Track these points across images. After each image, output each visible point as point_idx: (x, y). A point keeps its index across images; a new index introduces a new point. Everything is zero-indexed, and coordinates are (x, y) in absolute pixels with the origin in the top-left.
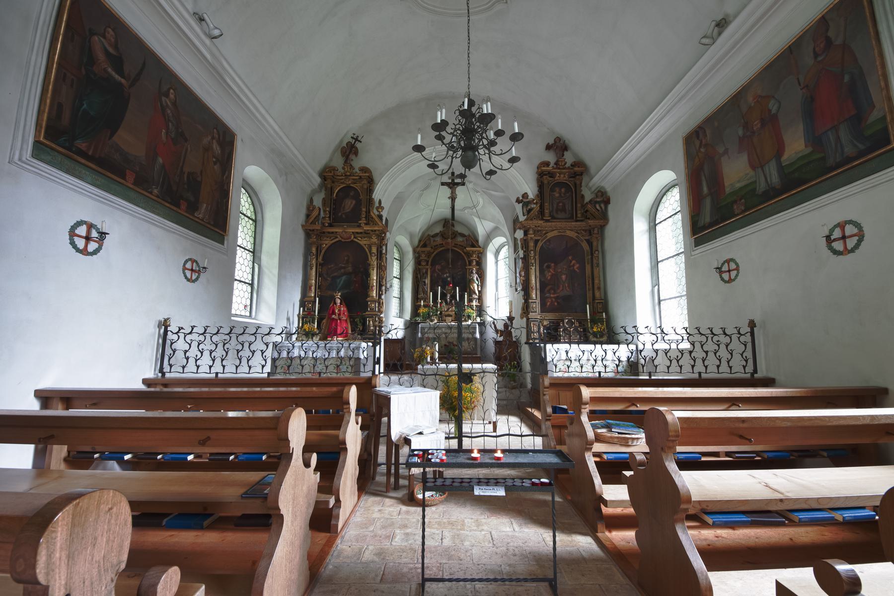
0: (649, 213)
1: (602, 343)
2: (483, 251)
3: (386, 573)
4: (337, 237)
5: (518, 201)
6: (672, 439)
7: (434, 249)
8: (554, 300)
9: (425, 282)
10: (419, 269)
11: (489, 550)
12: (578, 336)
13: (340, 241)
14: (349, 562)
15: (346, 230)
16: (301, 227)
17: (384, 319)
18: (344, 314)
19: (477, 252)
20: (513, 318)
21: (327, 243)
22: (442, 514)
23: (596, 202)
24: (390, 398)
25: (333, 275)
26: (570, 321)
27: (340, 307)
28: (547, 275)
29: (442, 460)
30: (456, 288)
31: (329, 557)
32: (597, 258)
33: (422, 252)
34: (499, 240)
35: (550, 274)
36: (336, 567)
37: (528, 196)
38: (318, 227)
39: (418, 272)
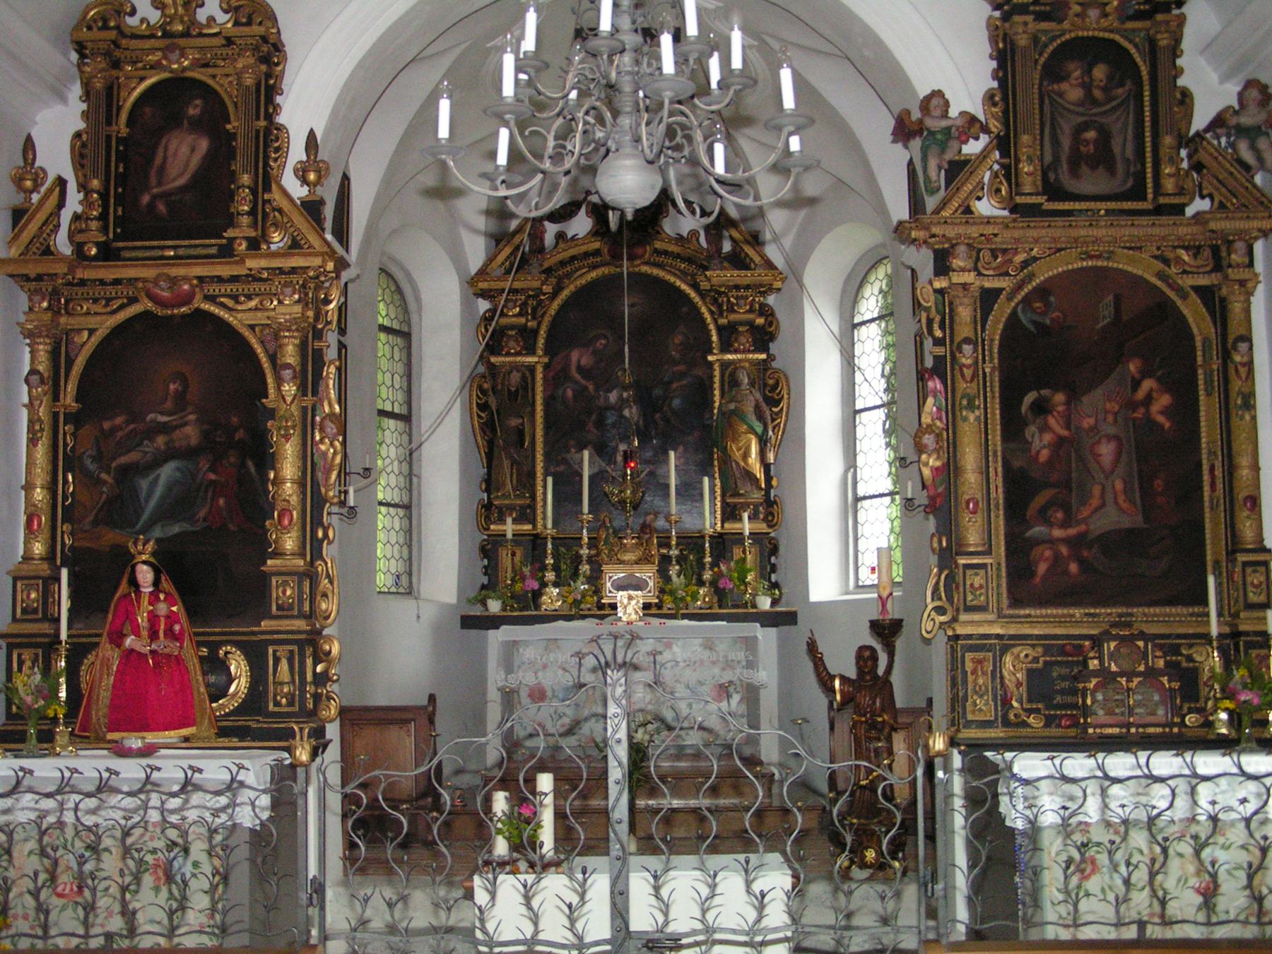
4: (133, 300)
8: (1064, 550)
25: (123, 460)
28: (1036, 444)
35: (1047, 437)
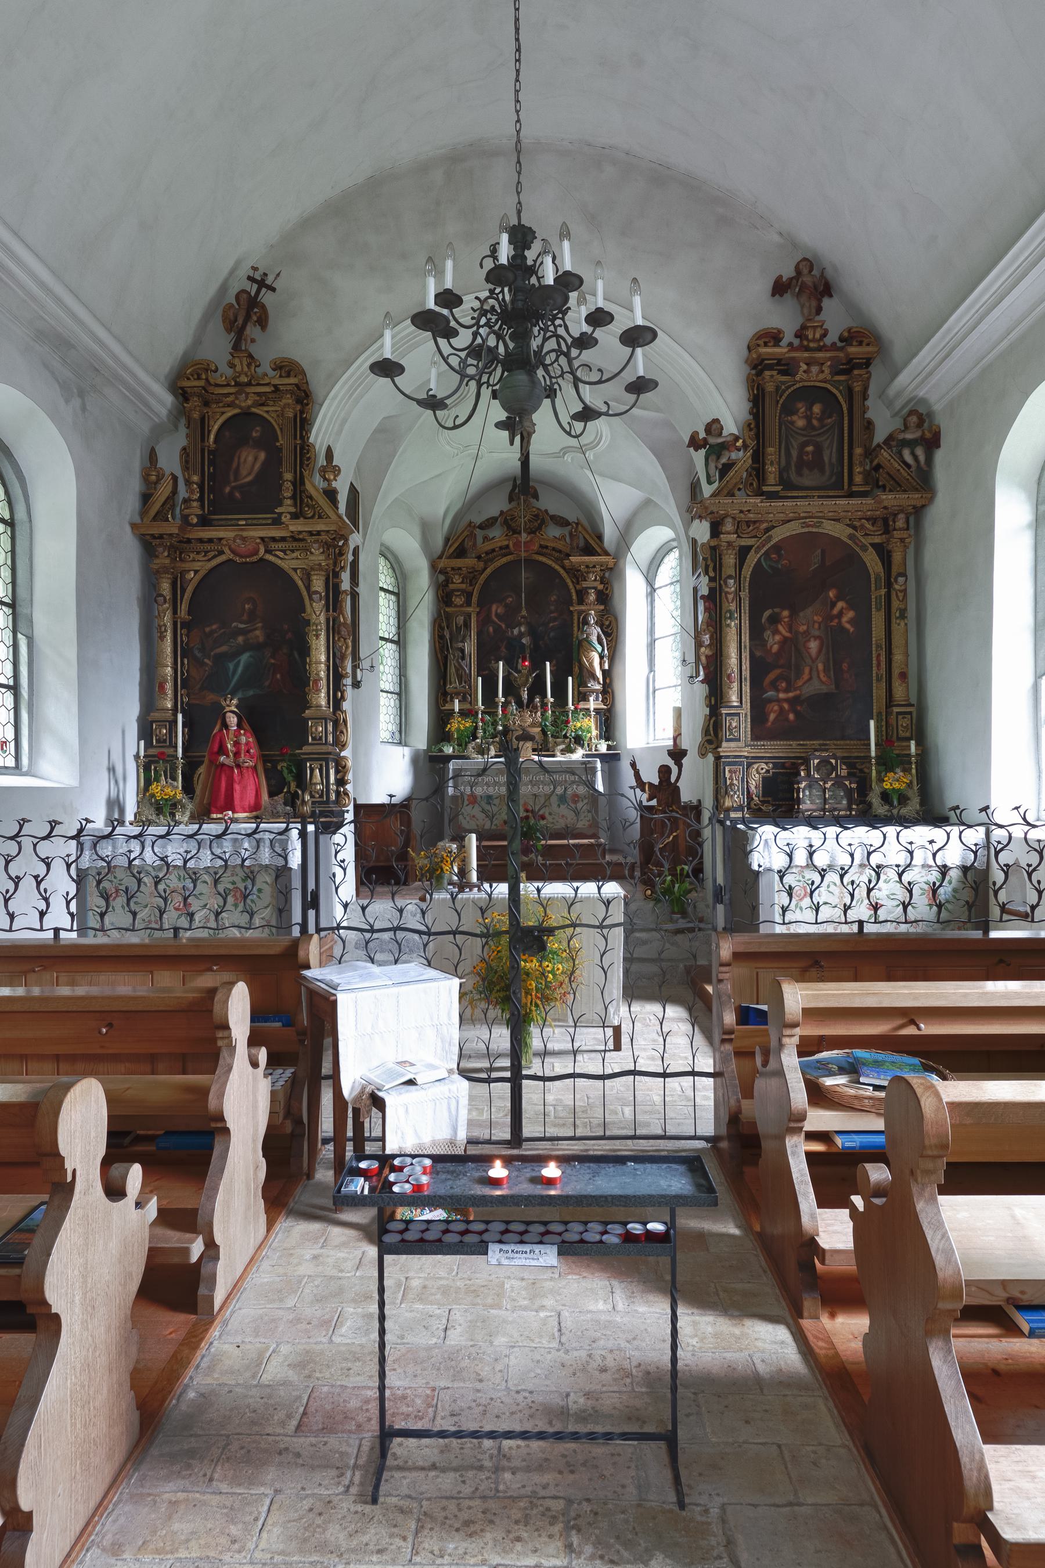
0: (1037, 476)
1: (905, 822)
2: (615, 564)
3: (311, 1409)
4: (222, 553)
5: (695, 443)
6: (930, 1153)
7: (486, 562)
8: (786, 706)
9: (462, 651)
10: (448, 617)
11: (549, 1357)
12: (845, 802)
13: (230, 560)
14: (233, 1382)
15: (245, 534)
16: (128, 529)
17: (350, 764)
18: (248, 751)
19: (598, 568)
20: (684, 753)
21: (196, 568)
22: (455, 1268)
23: (905, 443)
24: (335, 1002)
26: (824, 762)
27: (237, 734)
28: (771, 641)
29: (418, 1188)
30: (545, 665)
31: (190, 1371)
32: (901, 595)
33: (453, 569)
34: (656, 536)
35: (777, 638)
36: (203, 1395)
37: (722, 428)
38: (172, 527)
39: (444, 624)
